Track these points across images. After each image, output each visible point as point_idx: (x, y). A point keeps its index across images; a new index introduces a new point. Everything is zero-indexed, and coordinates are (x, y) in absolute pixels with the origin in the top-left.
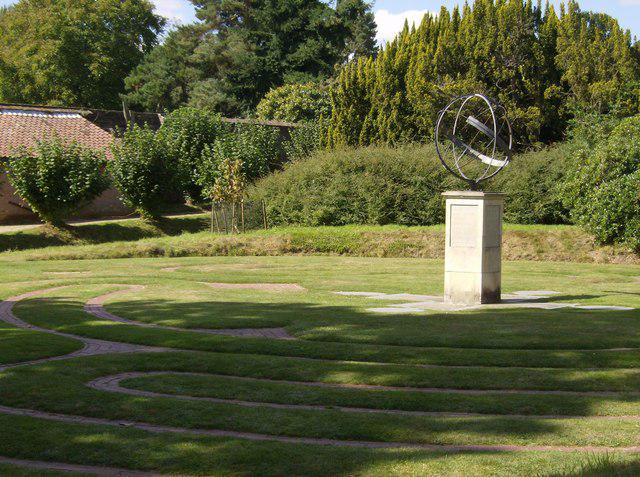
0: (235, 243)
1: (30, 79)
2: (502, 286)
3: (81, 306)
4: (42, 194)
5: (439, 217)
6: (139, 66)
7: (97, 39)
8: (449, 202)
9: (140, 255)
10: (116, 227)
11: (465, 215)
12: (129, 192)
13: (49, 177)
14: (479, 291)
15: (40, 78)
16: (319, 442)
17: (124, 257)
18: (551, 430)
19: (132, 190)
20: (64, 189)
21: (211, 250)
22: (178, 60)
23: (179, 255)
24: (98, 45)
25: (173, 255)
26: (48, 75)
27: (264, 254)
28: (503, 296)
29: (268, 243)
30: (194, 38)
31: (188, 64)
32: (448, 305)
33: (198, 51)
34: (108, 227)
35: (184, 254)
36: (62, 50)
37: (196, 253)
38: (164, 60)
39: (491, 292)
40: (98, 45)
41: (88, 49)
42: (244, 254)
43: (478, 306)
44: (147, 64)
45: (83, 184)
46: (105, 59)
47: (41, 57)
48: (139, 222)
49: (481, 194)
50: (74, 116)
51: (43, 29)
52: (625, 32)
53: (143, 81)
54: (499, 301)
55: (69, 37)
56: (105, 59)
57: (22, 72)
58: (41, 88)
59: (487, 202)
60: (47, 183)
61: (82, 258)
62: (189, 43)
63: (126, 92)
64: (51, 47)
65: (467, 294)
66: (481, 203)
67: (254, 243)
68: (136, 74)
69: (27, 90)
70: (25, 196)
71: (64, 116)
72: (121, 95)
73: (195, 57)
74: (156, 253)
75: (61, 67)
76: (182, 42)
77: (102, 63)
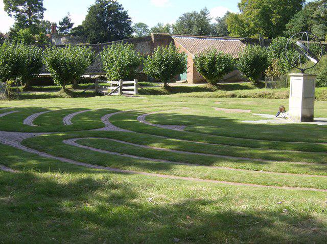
0: (267, 93)
1: (248, 25)
2: (315, 113)
3: (136, 111)
4: (207, 72)
5: (286, 84)
6: (292, 19)
7: (275, 8)
8: (291, 78)
9: (226, 96)
10: (239, 85)
11: (297, 83)
12: (244, 71)
13: (209, 64)
14: (300, 116)
15: (252, 25)
16: (110, 153)
17: (220, 97)
18: (266, 164)
19: (245, 71)
20: (215, 70)
21: (256, 96)
22: (308, 17)
23: (243, 97)
24: (275, 11)
25: (240, 97)
26: (255, 23)
27: (279, 98)
28: (314, 119)
29: (282, 94)
30: (315, 7)
31: (312, 18)
32: (289, 121)
33: (315, 13)
34: (234, 85)
35: (245, 97)
36: (261, 13)
37: (250, 97)
38: (302, 16)
39: (307, 117)
40: (275, 11)
41: (272, 13)
42: (270, 98)
43: (299, 122)
44: (295, 18)
45: (221, 68)
46: (278, 16)
47: (252, 16)
48: (249, 84)
49: (302, 74)
50: (236, 41)
51: (253, 5)
52: (158, 27)
53: (293, 26)
54: (312, 120)
55: (264, 7)
56: (278, 16)
57: (245, 22)
58: (252, 28)
59: (306, 78)
60: (208, 67)
61: (202, 97)
62: (312, 10)
63: (286, 30)
64: (256, 12)
65: (296, 117)
66: (302, 78)
67: (276, 93)
68: (290, 23)
69: (247, 30)
70: (200, 72)
71: (232, 41)
72: (283, 32)
73: (314, 16)
74: (233, 96)
75: (260, 19)
76: (309, 9)
77: (277, 18)
